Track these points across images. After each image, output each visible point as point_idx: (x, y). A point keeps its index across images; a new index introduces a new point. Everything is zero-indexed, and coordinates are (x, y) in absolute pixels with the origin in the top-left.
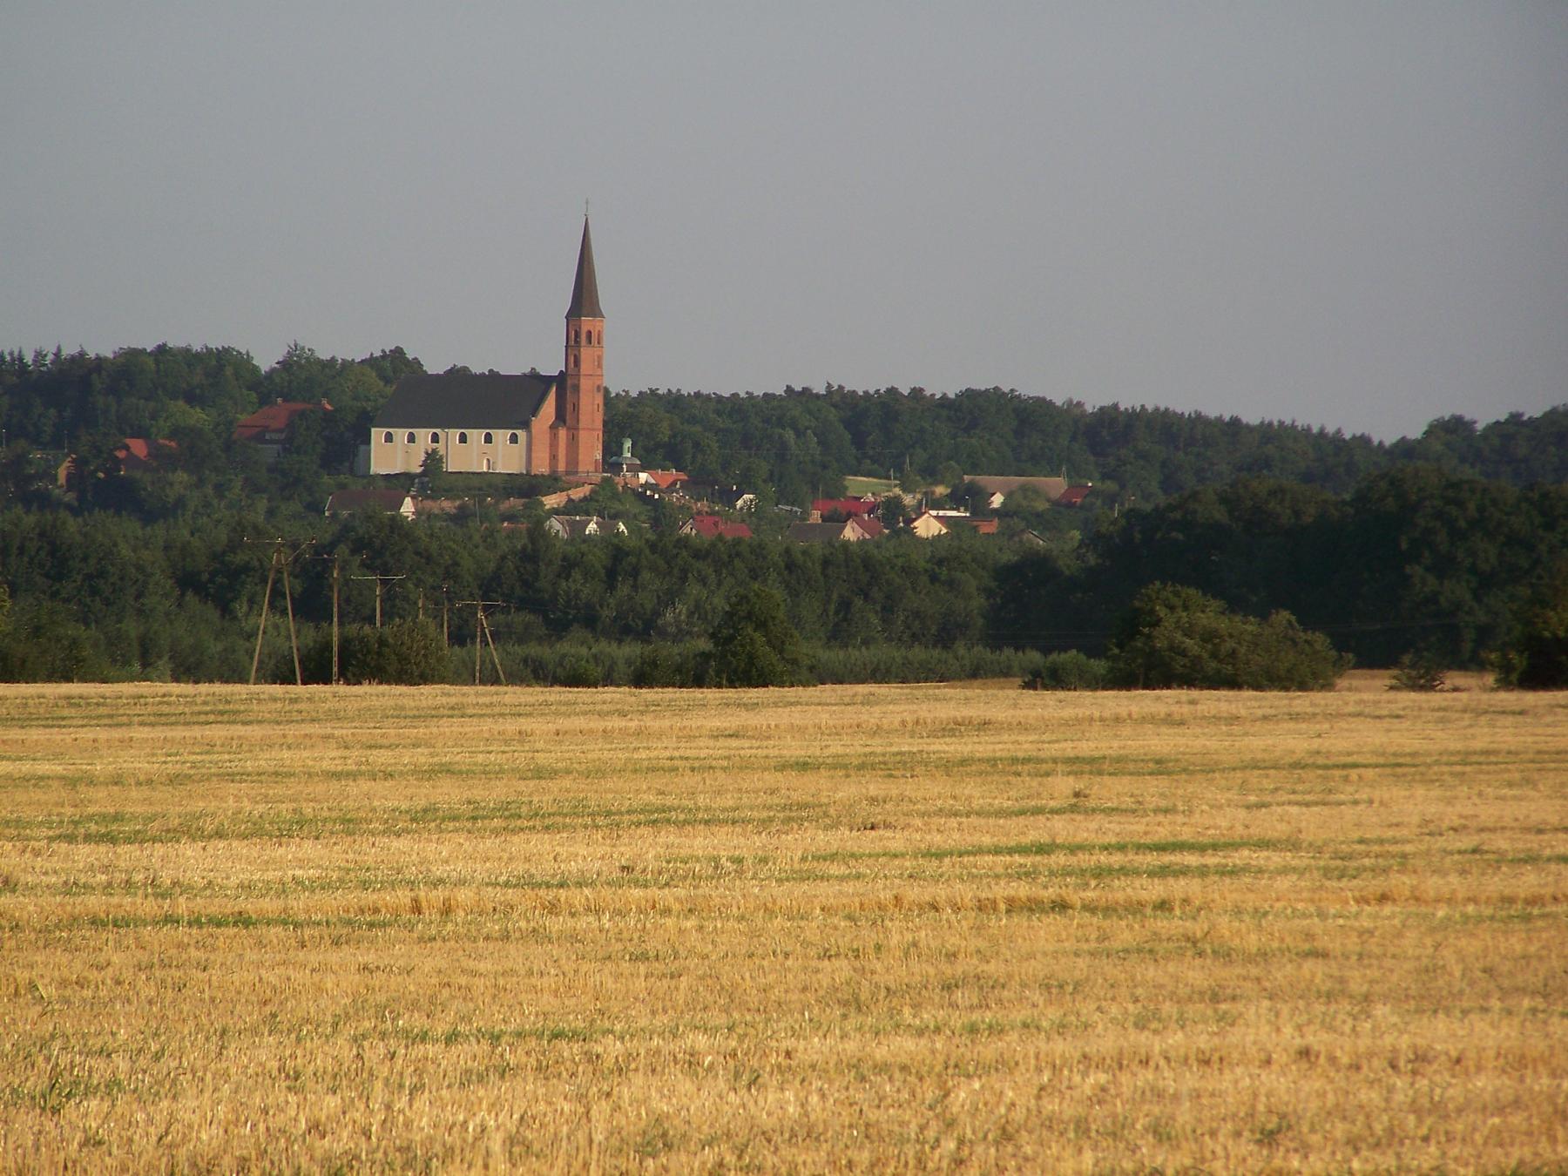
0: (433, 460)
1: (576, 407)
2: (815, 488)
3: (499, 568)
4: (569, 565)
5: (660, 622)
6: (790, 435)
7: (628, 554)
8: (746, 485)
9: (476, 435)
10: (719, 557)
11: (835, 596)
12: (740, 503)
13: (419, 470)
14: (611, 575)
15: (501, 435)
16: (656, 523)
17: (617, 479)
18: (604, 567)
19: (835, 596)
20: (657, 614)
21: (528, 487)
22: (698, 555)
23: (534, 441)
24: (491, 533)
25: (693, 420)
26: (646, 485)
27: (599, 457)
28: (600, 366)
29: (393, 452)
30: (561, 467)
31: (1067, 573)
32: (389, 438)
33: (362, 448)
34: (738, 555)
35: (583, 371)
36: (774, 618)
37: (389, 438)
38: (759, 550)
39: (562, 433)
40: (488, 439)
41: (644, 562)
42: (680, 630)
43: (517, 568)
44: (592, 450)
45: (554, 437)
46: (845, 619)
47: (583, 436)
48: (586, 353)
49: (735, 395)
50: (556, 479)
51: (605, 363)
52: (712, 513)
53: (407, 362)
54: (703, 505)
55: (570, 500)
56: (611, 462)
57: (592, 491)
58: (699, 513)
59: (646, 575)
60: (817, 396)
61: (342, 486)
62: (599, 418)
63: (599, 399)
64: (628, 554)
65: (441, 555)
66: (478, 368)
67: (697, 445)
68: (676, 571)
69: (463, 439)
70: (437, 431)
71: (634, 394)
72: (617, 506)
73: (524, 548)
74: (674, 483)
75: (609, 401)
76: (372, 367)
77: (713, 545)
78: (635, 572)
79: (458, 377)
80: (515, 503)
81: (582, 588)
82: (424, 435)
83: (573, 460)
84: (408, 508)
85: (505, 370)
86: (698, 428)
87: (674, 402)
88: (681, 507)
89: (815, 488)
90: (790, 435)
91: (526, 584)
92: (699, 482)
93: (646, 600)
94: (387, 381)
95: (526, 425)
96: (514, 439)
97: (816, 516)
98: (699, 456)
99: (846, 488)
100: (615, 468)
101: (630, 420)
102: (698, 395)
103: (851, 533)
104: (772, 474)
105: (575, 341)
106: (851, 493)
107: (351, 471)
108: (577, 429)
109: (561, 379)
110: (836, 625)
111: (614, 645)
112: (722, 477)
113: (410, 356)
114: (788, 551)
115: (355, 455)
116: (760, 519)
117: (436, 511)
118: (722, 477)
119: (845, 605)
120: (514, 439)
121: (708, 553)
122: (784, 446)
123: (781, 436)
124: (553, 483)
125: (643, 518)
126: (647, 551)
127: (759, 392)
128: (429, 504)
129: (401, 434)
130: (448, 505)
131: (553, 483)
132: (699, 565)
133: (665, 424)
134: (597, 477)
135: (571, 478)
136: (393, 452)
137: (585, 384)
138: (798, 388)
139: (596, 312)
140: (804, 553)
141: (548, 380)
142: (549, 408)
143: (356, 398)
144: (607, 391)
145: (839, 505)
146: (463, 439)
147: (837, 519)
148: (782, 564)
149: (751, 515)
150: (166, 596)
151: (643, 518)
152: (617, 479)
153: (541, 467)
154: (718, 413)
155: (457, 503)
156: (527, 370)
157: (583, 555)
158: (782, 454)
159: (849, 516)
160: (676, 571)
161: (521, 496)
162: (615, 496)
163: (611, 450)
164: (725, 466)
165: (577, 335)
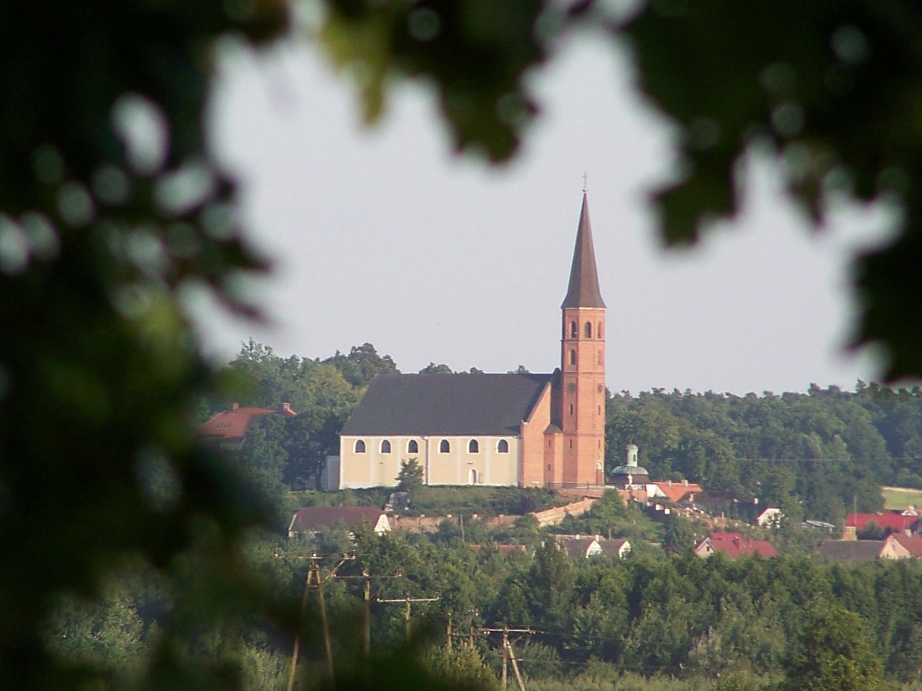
0: (411, 473)
1: (574, 410)
2: (848, 500)
3: (504, 592)
4: (584, 592)
5: (691, 653)
6: (815, 441)
7: (652, 576)
8: (770, 497)
9: (460, 443)
10: (757, 580)
11: (892, 623)
12: (762, 519)
13: (396, 484)
14: (635, 603)
15: (489, 443)
16: (668, 543)
17: (621, 492)
18: (626, 591)
19: (892, 623)
20: (690, 646)
21: (521, 502)
22: (732, 575)
23: (526, 448)
24: (486, 556)
25: (704, 424)
26: (655, 499)
27: (601, 467)
28: (601, 363)
29: (365, 463)
30: (558, 479)
31: (573, 569)
32: (361, 447)
33: (330, 459)
34: (778, 575)
35: (581, 369)
36: (854, 645)
37: (361, 447)
38: (802, 570)
39: (559, 440)
40: (474, 447)
41: (671, 584)
42: (713, 663)
43: (525, 593)
44: (592, 458)
45: (550, 444)
46: (903, 649)
47: (582, 443)
48: (585, 348)
49: (751, 395)
50: (552, 493)
51: (607, 359)
52: (730, 530)
53: (376, 361)
54: (720, 522)
55: (569, 517)
56: (615, 474)
57: (594, 507)
58: (717, 530)
59: (677, 602)
60: (847, 396)
61: (310, 503)
62: (601, 422)
63: (601, 401)
64: (652, 576)
65: (438, 579)
66: (459, 366)
67: (710, 452)
68: (707, 595)
69: (445, 447)
70: (416, 438)
71: (635, 395)
72: (622, 523)
73: (533, 571)
74: (686, 496)
75: (611, 405)
76: (338, 367)
77: (750, 566)
78: (662, 597)
79: (435, 377)
80: (506, 520)
81: (602, 616)
82: (400, 443)
83: (571, 470)
84: (383, 525)
85: (488, 369)
86: (710, 433)
87: (684, 405)
88: (696, 524)
89: (848, 500)
90: (815, 441)
91: (536, 612)
92: (715, 494)
93: (678, 630)
94: (356, 383)
95: (516, 431)
96: (503, 447)
97: (850, 534)
98: (714, 466)
99: (883, 500)
100: (620, 479)
101: (632, 425)
102: (709, 395)
103: (892, 550)
104: (799, 483)
105: (572, 334)
106: (889, 506)
107: (319, 487)
108: (576, 435)
109: (557, 378)
110: (892, 655)
111: (643, 680)
112: (740, 488)
113: (381, 354)
114: (835, 571)
115: (322, 468)
116: (787, 537)
117: (415, 530)
118: (740, 488)
119: (904, 633)
120: (503, 447)
121: (744, 575)
122: (809, 453)
123: (805, 441)
124: (547, 497)
125: (653, 536)
126: (675, 573)
127: (778, 392)
128: (406, 522)
129: (374, 443)
130: (430, 524)
131: (547, 497)
132: (733, 587)
133: (675, 429)
134: (599, 491)
135: (571, 491)
136: (365, 463)
137: (584, 384)
138: (824, 387)
139: (596, 301)
140: (855, 573)
141: (542, 380)
142: (543, 411)
143: (320, 403)
144: (607, 393)
145: (875, 520)
146: (445, 447)
147: (874, 536)
148: (829, 587)
149: (775, 532)
150: (127, 628)
151: (653, 536)
152: (621, 492)
153: (535, 480)
154: (733, 415)
155: (439, 521)
156: (514, 369)
157: (600, 577)
158: (808, 461)
159: (888, 532)
160: (707, 595)
161: (512, 512)
162: (620, 512)
163: (614, 457)
164: (745, 474)
165: (575, 327)
